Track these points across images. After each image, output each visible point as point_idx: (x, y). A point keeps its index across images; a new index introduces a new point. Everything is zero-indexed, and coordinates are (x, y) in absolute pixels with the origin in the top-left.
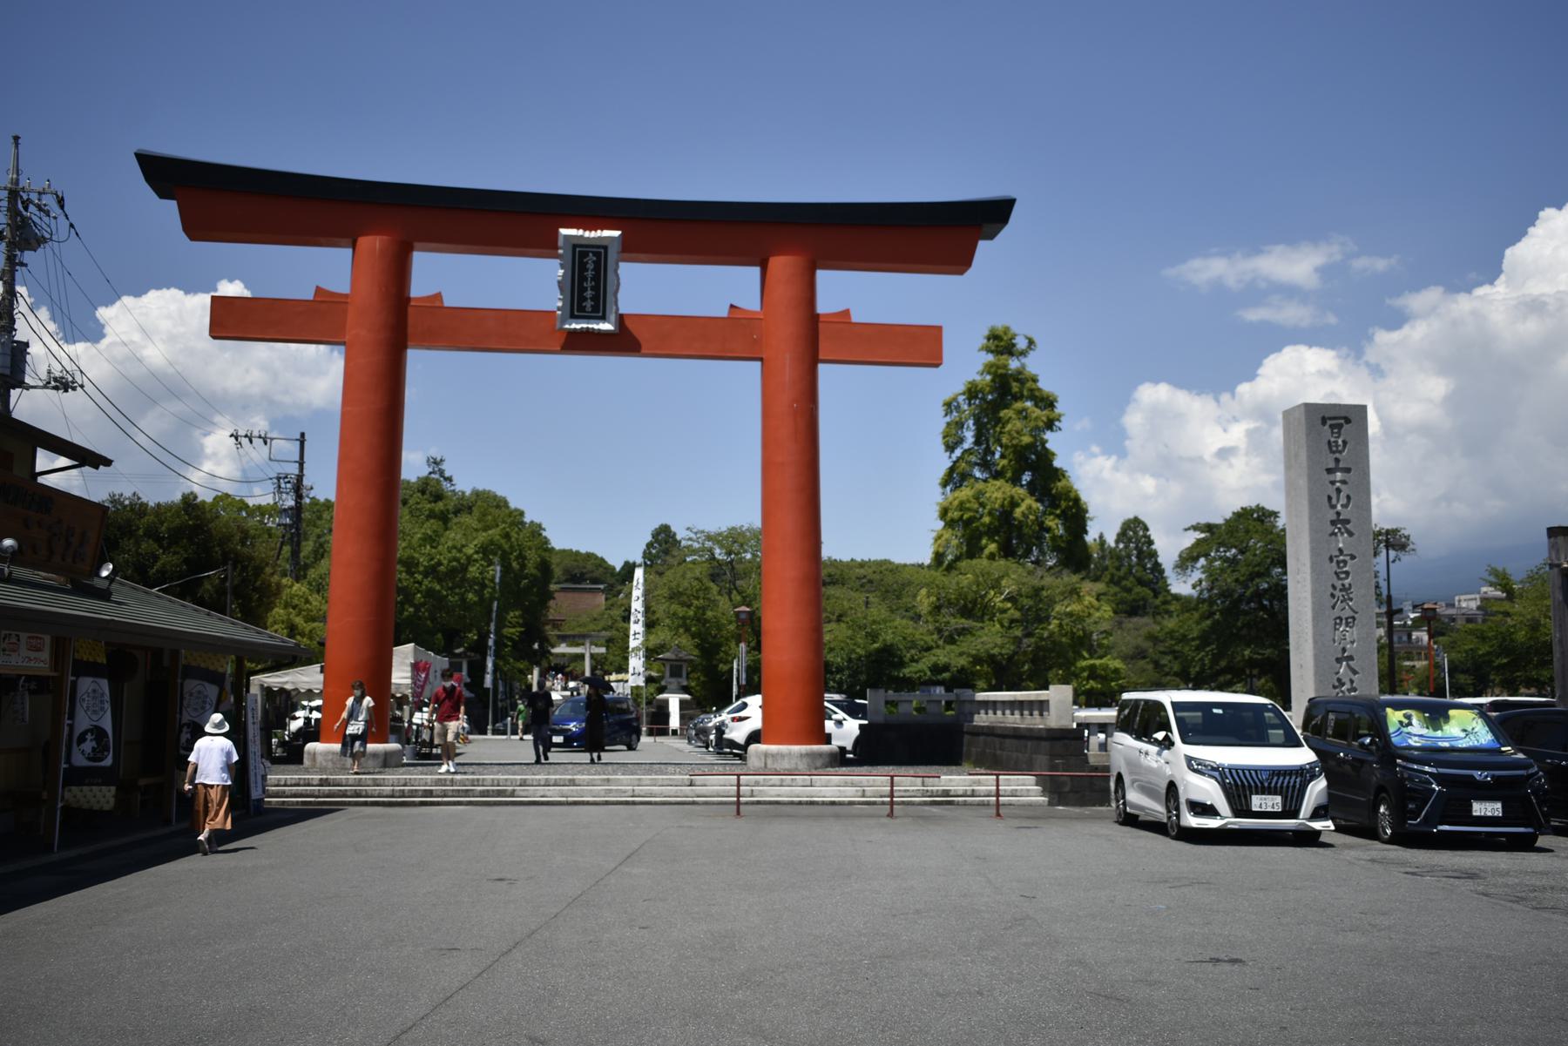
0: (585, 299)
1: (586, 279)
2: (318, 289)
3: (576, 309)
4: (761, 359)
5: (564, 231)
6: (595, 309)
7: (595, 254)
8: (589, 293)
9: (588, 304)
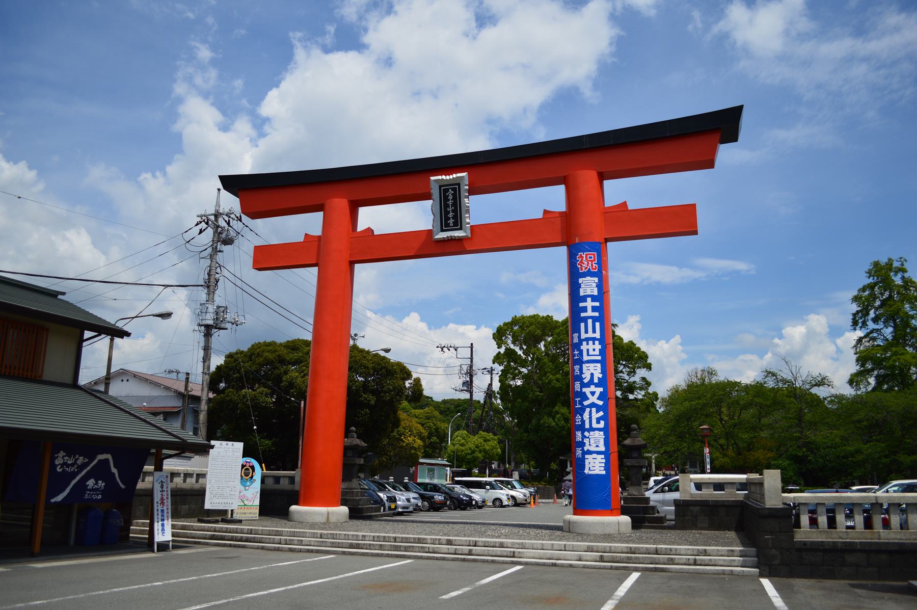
2: (545, 212)
4: (352, 263)
5: (432, 178)
6: (455, 224)
7: (452, 189)
8: (451, 215)
9: (451, 221)
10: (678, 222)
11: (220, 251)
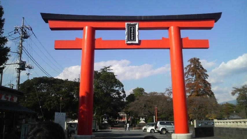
0: (132, 37)
1: (131, 33)
2: (163, 38)
3: (129, 39)
6: (134, 39)
8: (132, 36)
9: (132, 38)
10: (203, 45)
11: (24, 41)
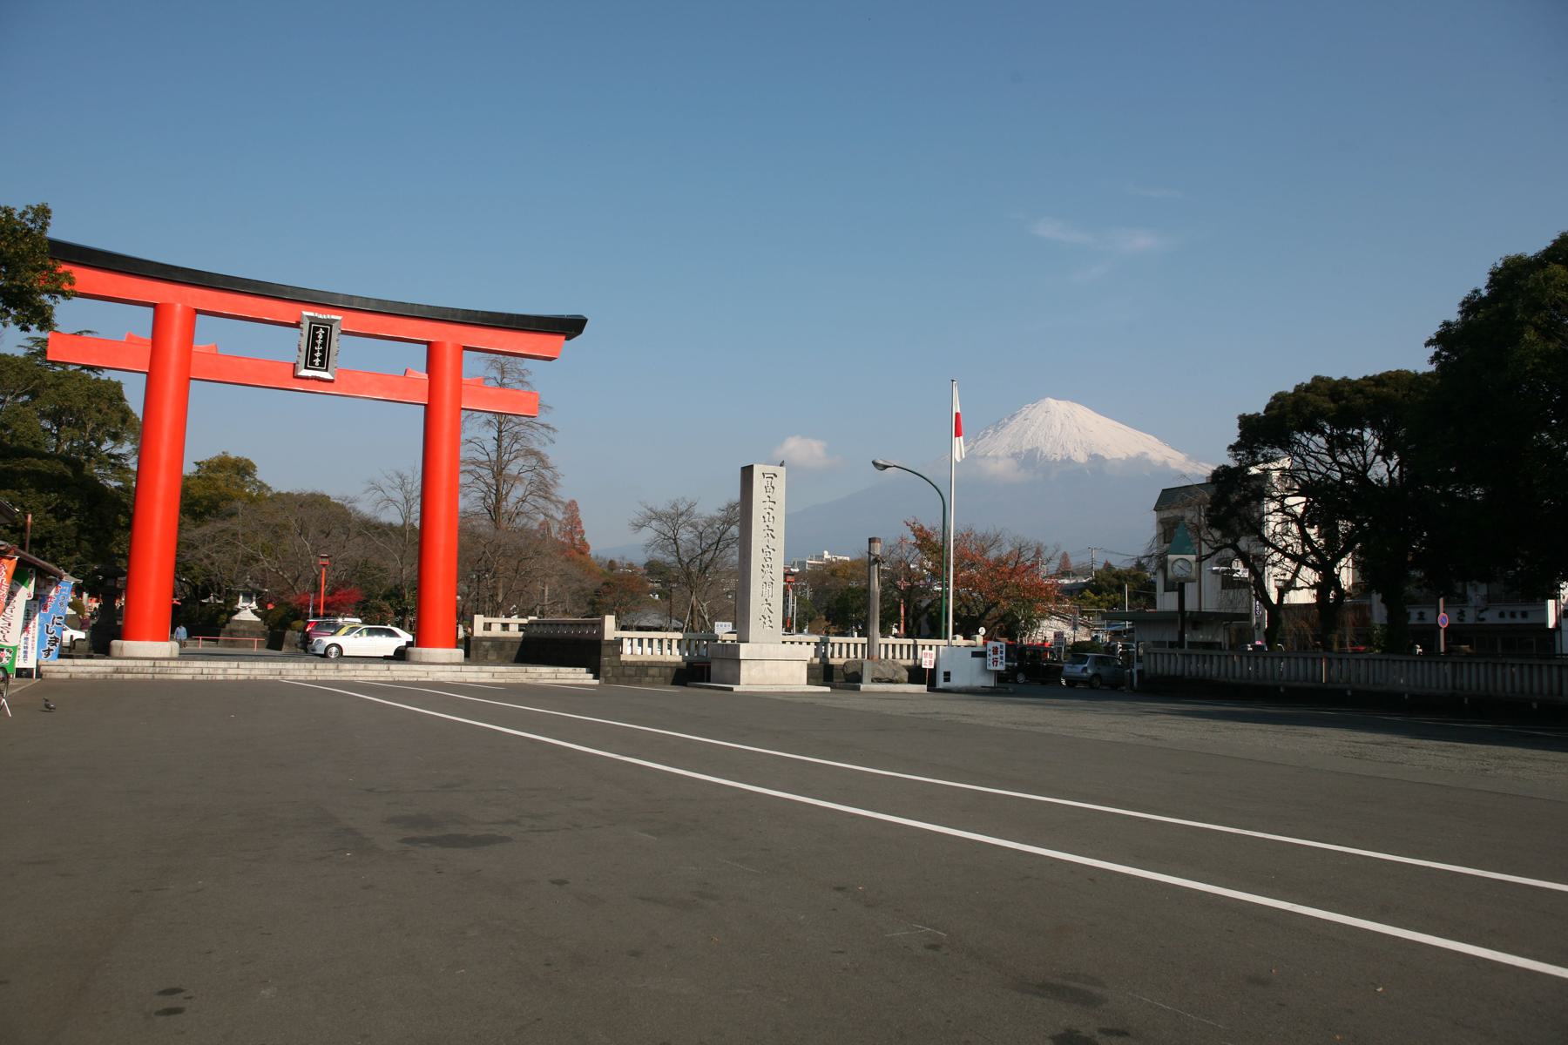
6: (321, 364)
